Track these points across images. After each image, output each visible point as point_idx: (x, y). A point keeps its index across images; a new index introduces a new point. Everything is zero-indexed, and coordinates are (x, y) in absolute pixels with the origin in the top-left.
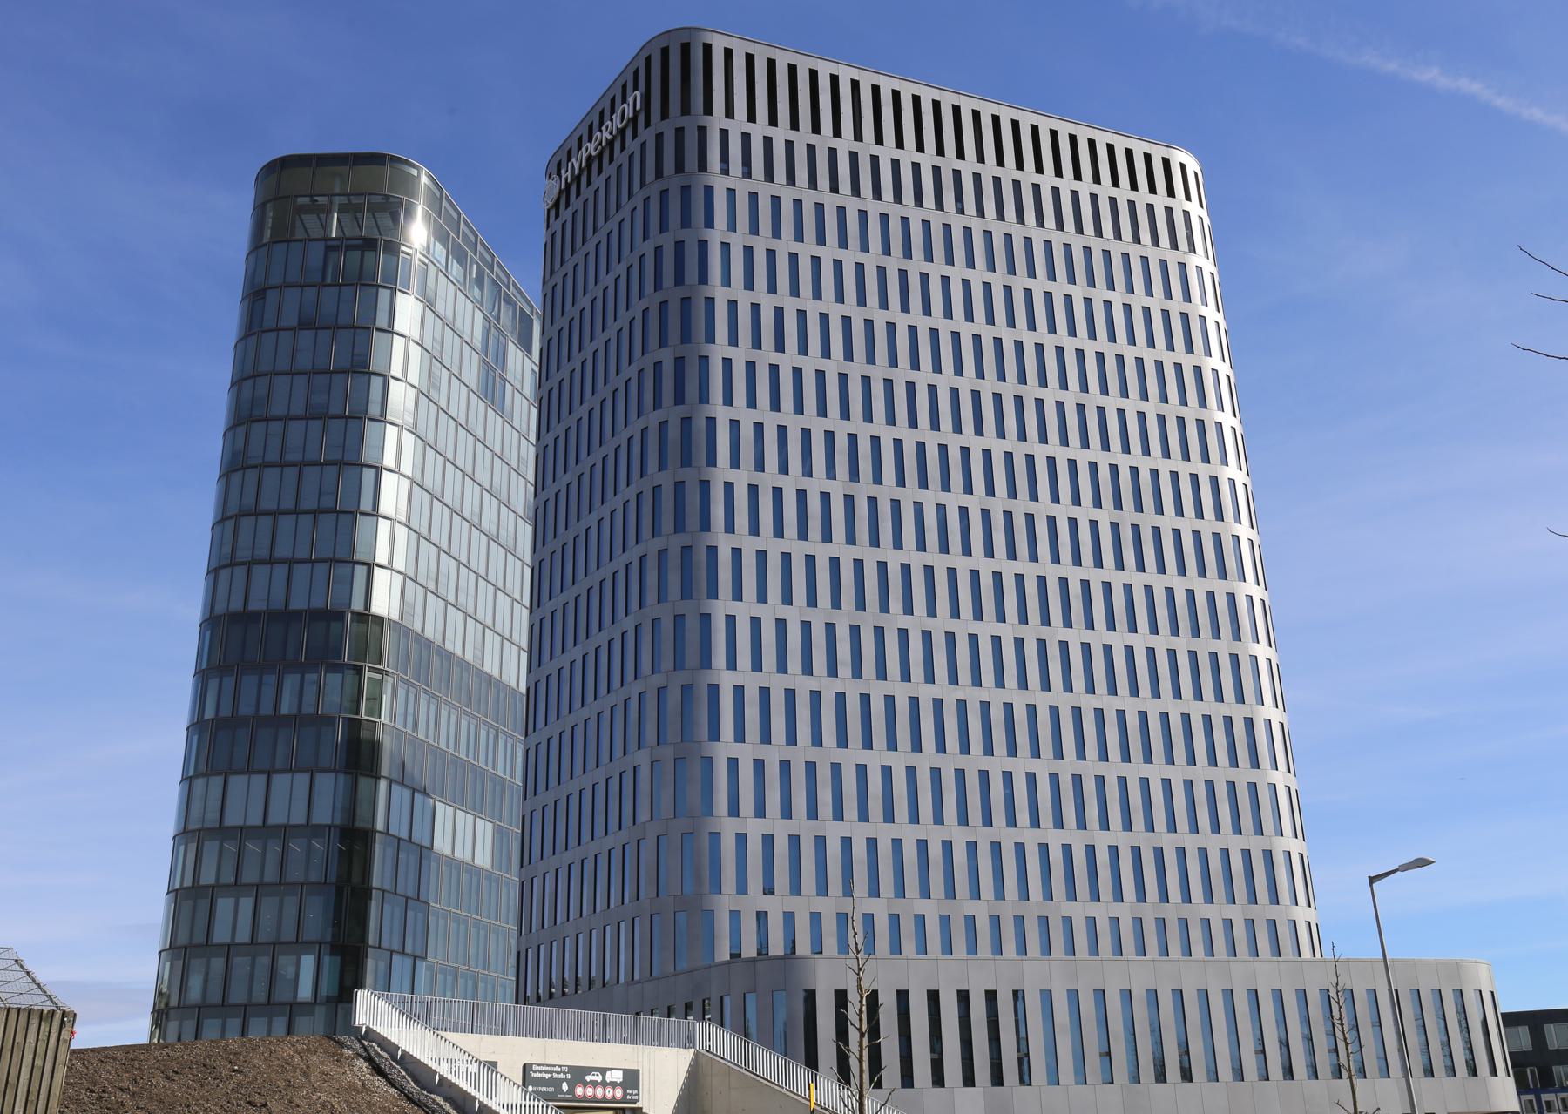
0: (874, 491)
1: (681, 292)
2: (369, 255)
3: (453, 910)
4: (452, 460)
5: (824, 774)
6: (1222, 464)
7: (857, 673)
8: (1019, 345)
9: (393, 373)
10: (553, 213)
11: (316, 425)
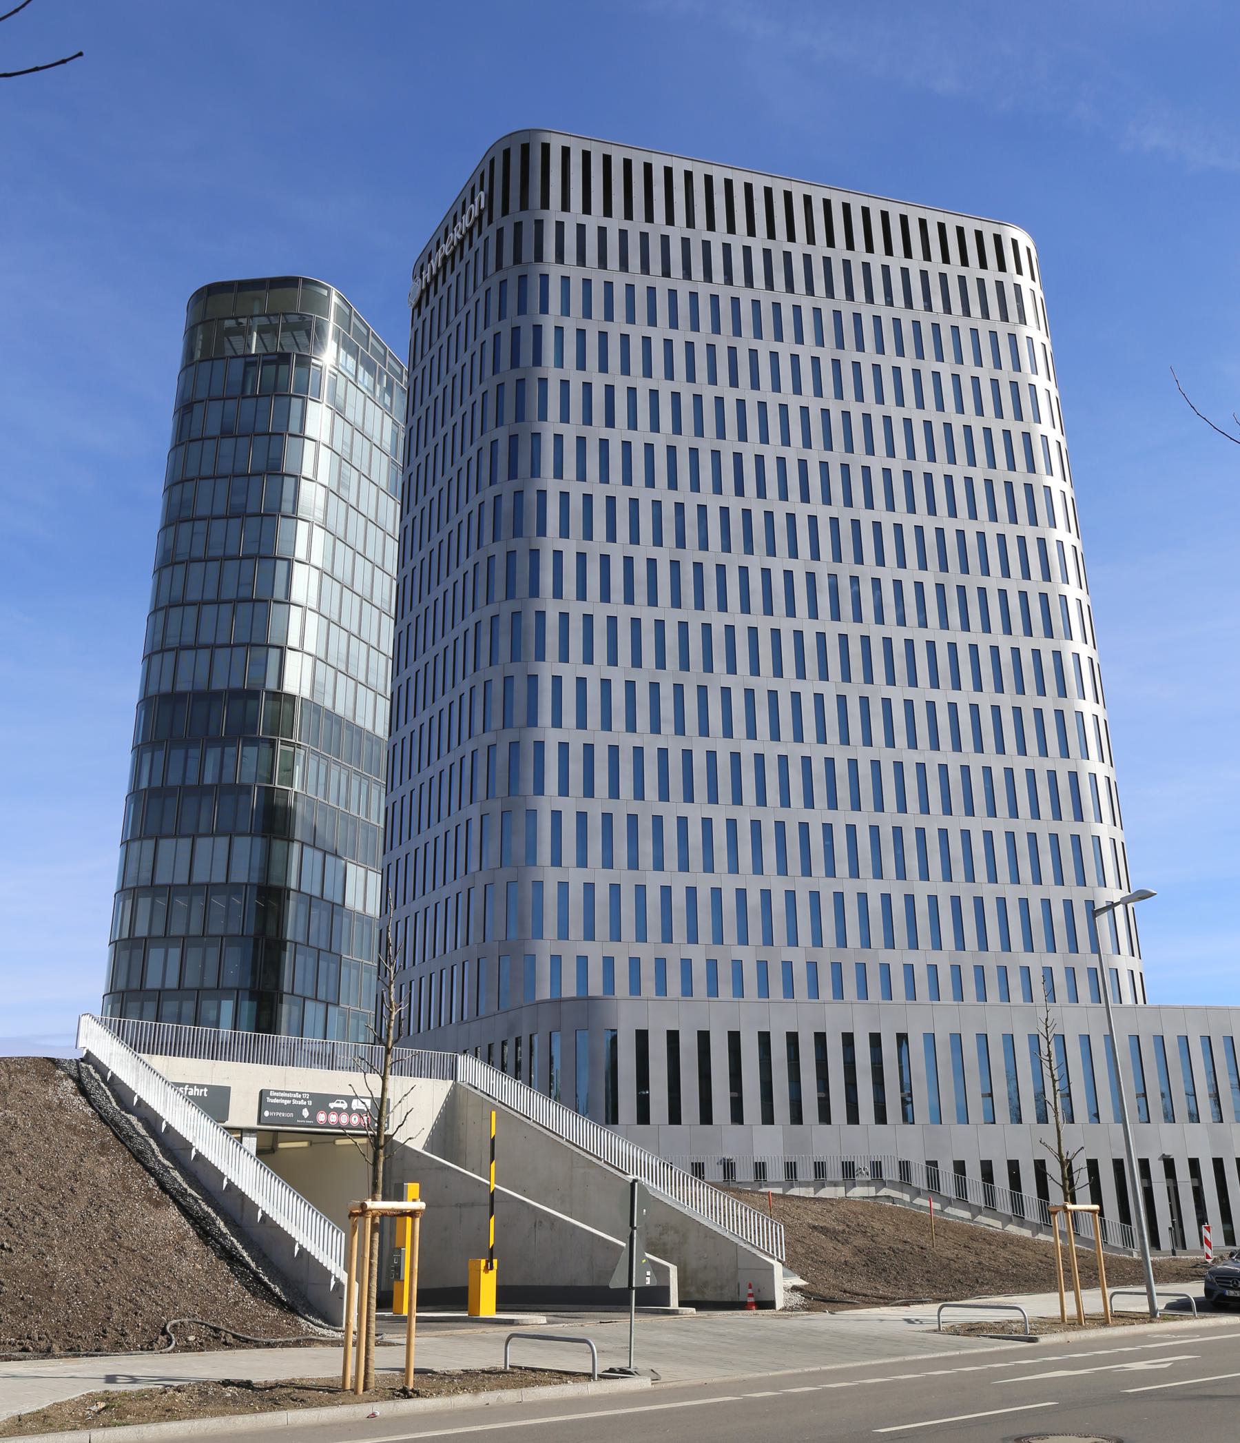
0: (700, 556)
1: (517, 374)
2: (283, 368)
3: (365, 962)
4: (362, 552)
5: (645, 827)
6: (1050, 527)
7: (680, 729)
8: (846, 415)
9: (304, 474)
10: (416, 311)
11: (235, 523)
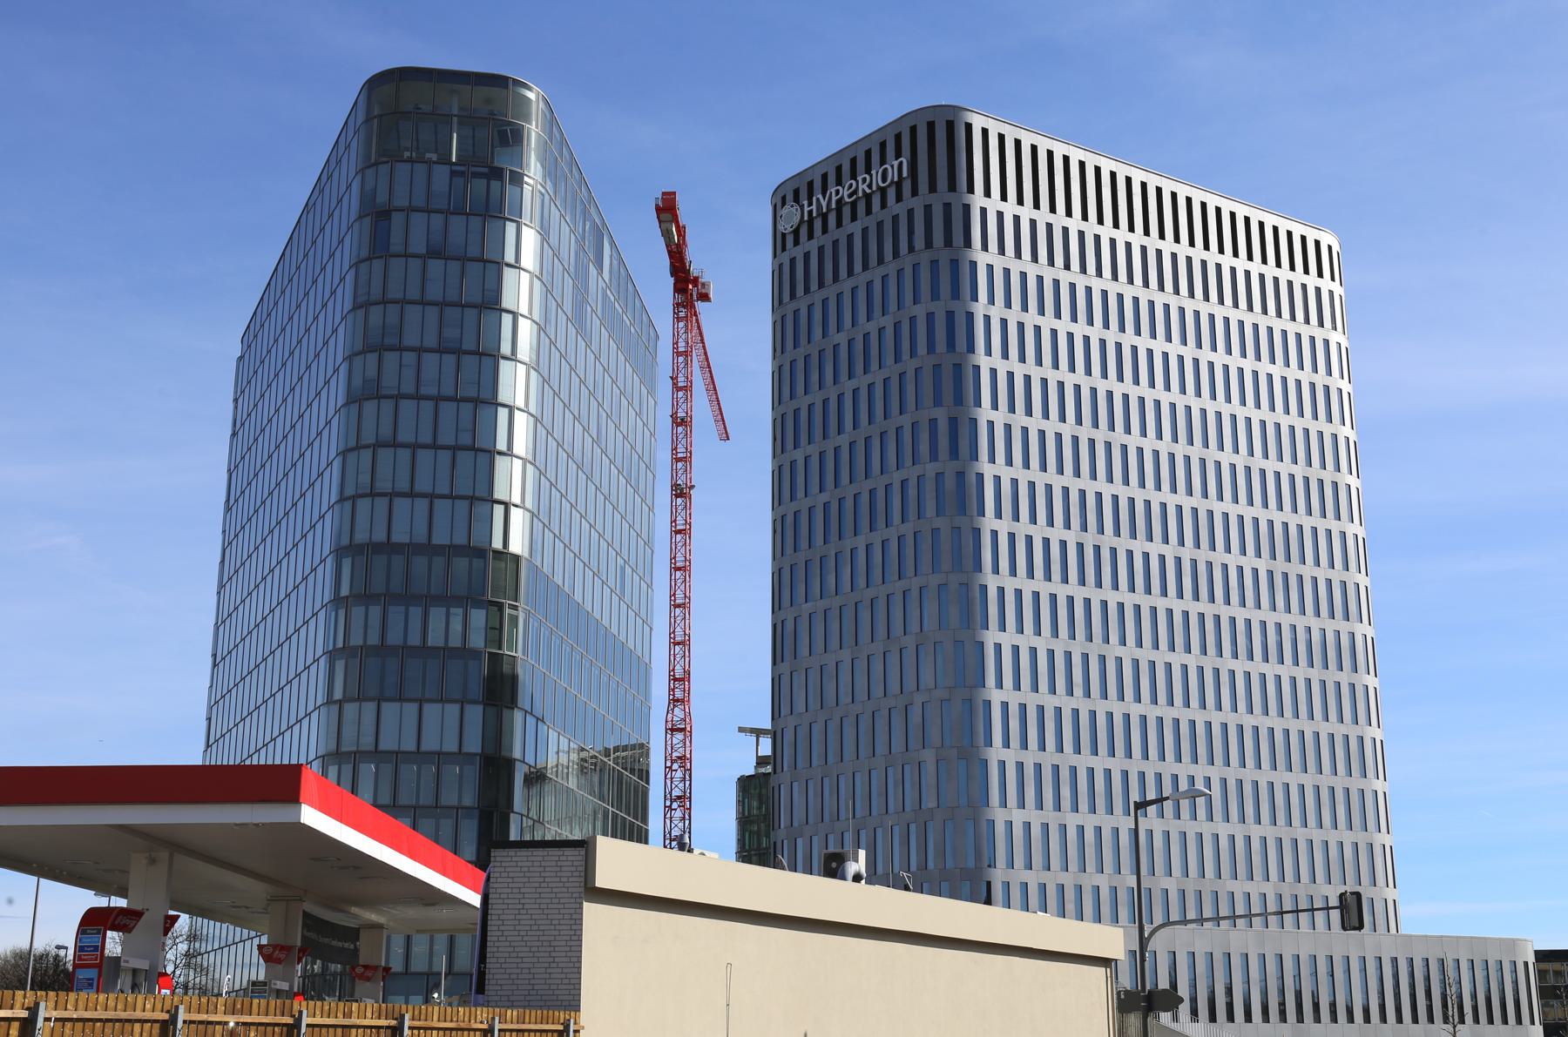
2: (495, 185)
